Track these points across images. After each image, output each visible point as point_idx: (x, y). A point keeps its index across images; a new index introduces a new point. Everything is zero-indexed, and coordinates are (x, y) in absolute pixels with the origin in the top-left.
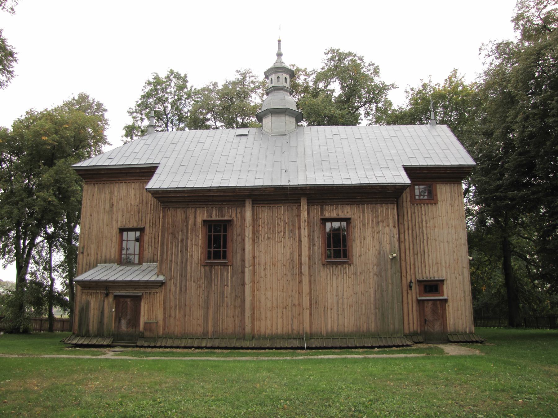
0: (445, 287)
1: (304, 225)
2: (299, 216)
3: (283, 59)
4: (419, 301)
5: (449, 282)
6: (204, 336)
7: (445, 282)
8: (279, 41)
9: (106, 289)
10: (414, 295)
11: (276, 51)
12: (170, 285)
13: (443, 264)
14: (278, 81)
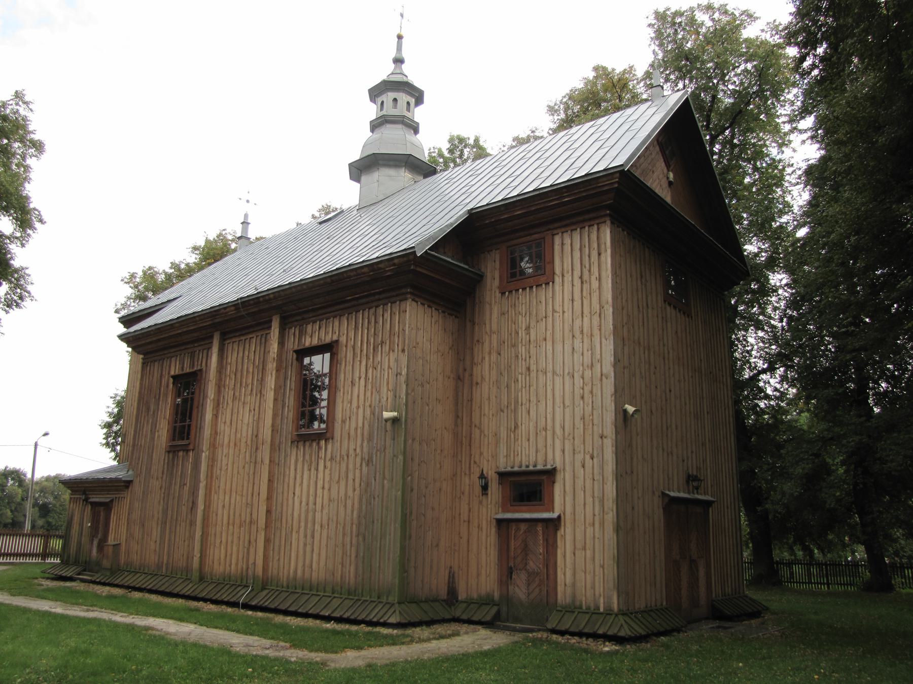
0: (558, 489)
1: (271, 366)
2: (266, 353)
3: (405, 68)
4: (500, 522)
5: (568, 476)
6: (241, 582)
7: (559, 477)
8: (400, 37)
9: (84, 493)
10: (491, 508)
11: (393, 54)
12: (137, 488)
13: (558, 431)
14: (395, 106)
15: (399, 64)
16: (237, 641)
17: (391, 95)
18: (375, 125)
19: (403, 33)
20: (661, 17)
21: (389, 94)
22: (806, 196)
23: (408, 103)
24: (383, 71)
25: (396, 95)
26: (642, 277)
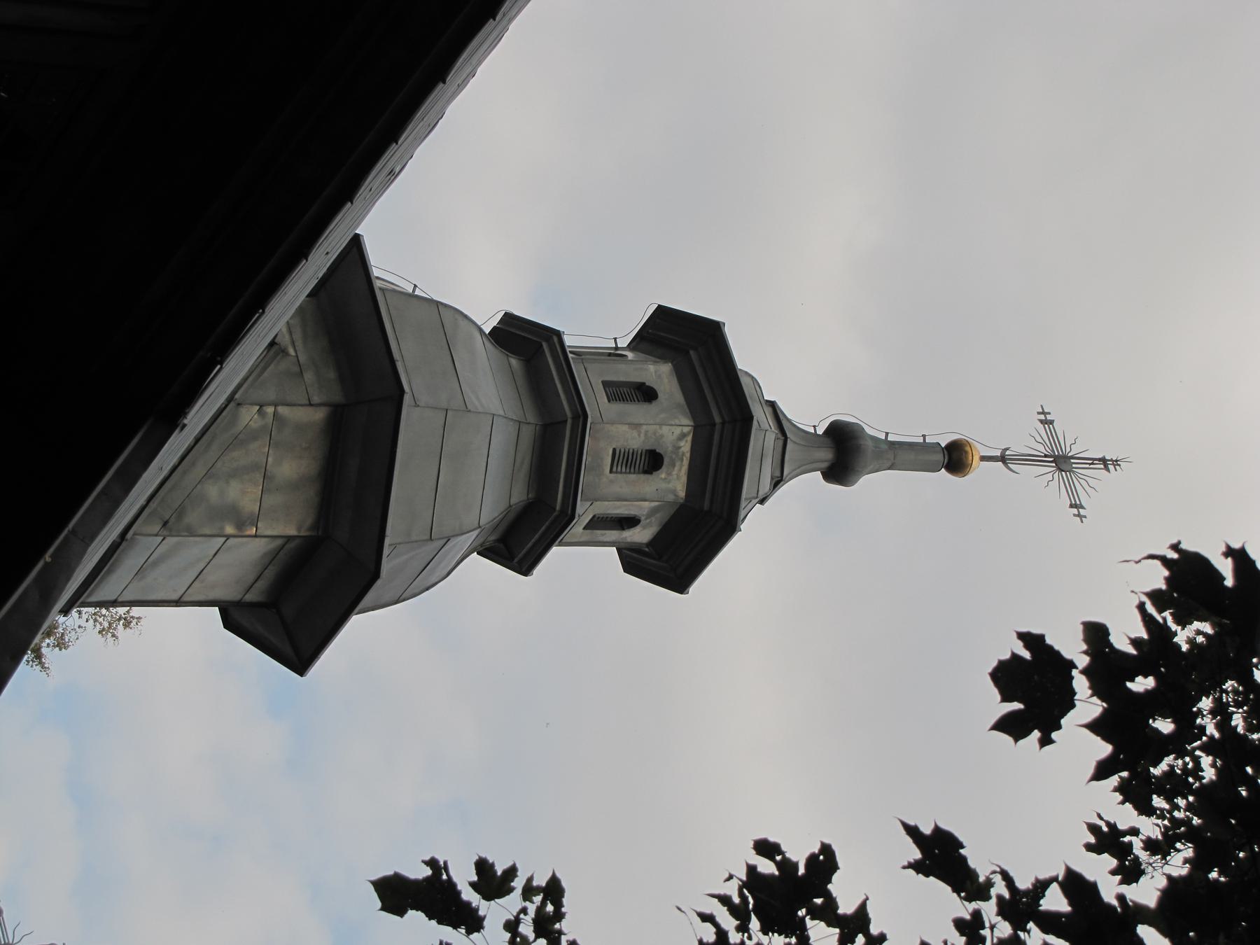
8: (955, 458)
14: (626, 461)
15: (826, 455)
17: (673, 482)
18: (522, 340)
19: (980, 471)
20: (300, 662)
23: (629, 522)
24: (792, 375)
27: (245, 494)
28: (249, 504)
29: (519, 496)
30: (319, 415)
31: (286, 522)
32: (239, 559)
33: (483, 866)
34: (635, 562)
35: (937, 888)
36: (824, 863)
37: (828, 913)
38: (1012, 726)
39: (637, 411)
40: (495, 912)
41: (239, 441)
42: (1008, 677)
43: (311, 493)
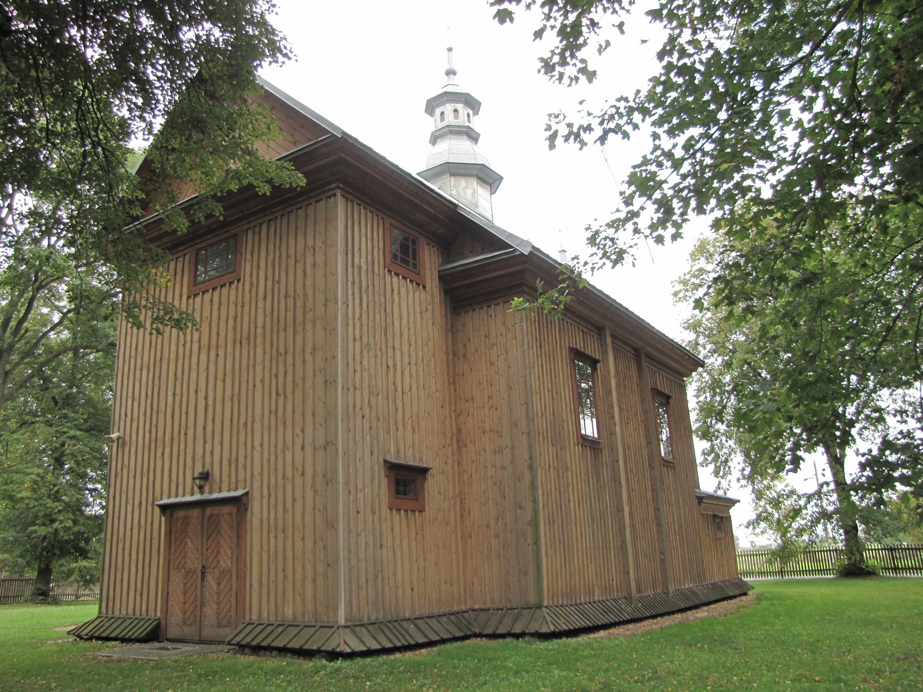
14: (456, 117)
15: (451, 76)
16: (340, 466)
17: (460, 107)
18: (435, 139)
20: (502, 178)
21: (448, 105)
22: (163, 121)
23: (468, 115)
25: (581, 149)
26: (541, 347)
27: (469, 192)
28: (471, 191)
29: (465, 137)
30: (452, 178)
31: (474, 183)
32: (482, 193)
33: (546, 130)
34: (476, 113)
35: (545, 35)
36: (542, 60)
37: (551, 58)
38: (512, 20)
39: (446, 115)
40: (554, 128)
41: (459, 193)
42: (502, 21)
43: (468, 179)
